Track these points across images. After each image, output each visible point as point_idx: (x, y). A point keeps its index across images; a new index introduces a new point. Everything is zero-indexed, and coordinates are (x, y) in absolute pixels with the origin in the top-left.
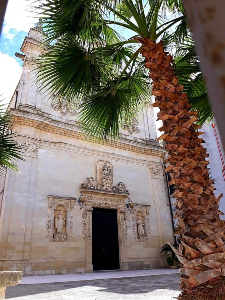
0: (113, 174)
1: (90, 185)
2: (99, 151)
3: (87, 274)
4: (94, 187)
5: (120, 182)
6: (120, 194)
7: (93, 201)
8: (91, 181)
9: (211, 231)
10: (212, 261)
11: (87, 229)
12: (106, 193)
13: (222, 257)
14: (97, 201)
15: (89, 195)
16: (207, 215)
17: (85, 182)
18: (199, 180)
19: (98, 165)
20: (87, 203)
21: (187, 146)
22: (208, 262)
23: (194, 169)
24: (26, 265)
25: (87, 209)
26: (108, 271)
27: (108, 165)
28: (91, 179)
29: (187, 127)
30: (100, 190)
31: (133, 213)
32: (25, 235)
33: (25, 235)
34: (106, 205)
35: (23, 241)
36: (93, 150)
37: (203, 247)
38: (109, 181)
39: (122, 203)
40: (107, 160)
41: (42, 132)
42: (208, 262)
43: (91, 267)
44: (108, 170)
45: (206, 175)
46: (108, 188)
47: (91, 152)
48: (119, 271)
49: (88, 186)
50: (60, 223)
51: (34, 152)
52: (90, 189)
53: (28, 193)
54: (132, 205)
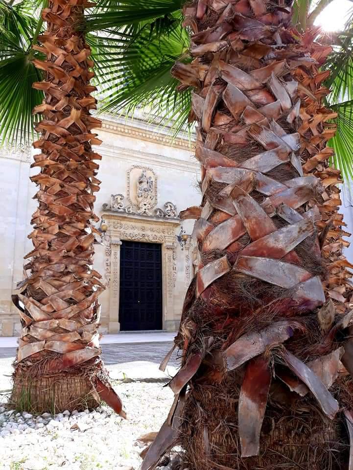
0: (157, 190)
1: (116, 206)
2: (134, 151)
3: (109, 335)
4: (125, 210)
5: (168, 203)
6: (167, 221)
7: (122, 230)
8: (119, 199)
9: (53, 288)
10: (42, 330)
11: (111, 272)
12: (144, 218)
13: (56, 326)
14: (128, 231)
15: (116, 221)
16: (55, 266)
17: (110, 201)
18: (59, 213)
20: (111, 234)
21: (55, 157)
22: (37, 331)
23: (56, 195)
24: (15, 322)
25: (112, 242)
26: (143, 332)
27: (149, 174)
28: (119, 197)
29: (65, 125)
30: (134, 214)
31: (188, 249)
32: (13, 280)
33: (13, 280)
34: (144, 237)
35: (10, 288)
36: (124, 149)
37: (34, 311)
38: (148, 200)
39: (171, 234)
40: (147, 166)
42: (37, 331)
43: (117, 325)
44: (147, 183)
45: (76, 205)
46: (147, 211)
47: (118, 152)
48: (161, 332)
49: (113, 207)
51: (23, 152)
52: (117, 212)
53: (16, 218)
54: (185, 237)
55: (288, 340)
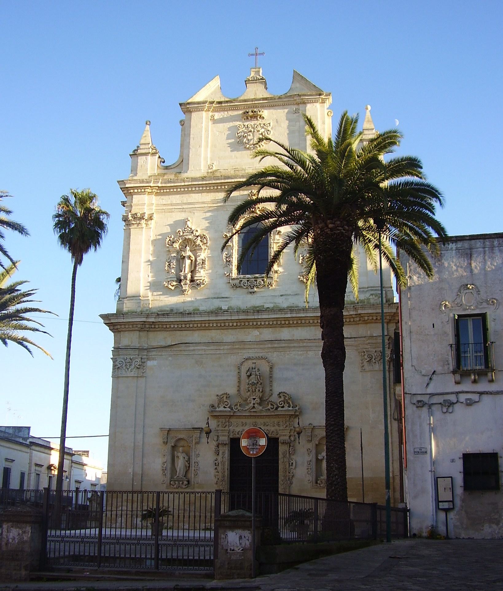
5: (280, 393)
19: (263, 361)
41: (151, 334)
47: (229, 347)
50: (180, 464)
55: (350, 257)
